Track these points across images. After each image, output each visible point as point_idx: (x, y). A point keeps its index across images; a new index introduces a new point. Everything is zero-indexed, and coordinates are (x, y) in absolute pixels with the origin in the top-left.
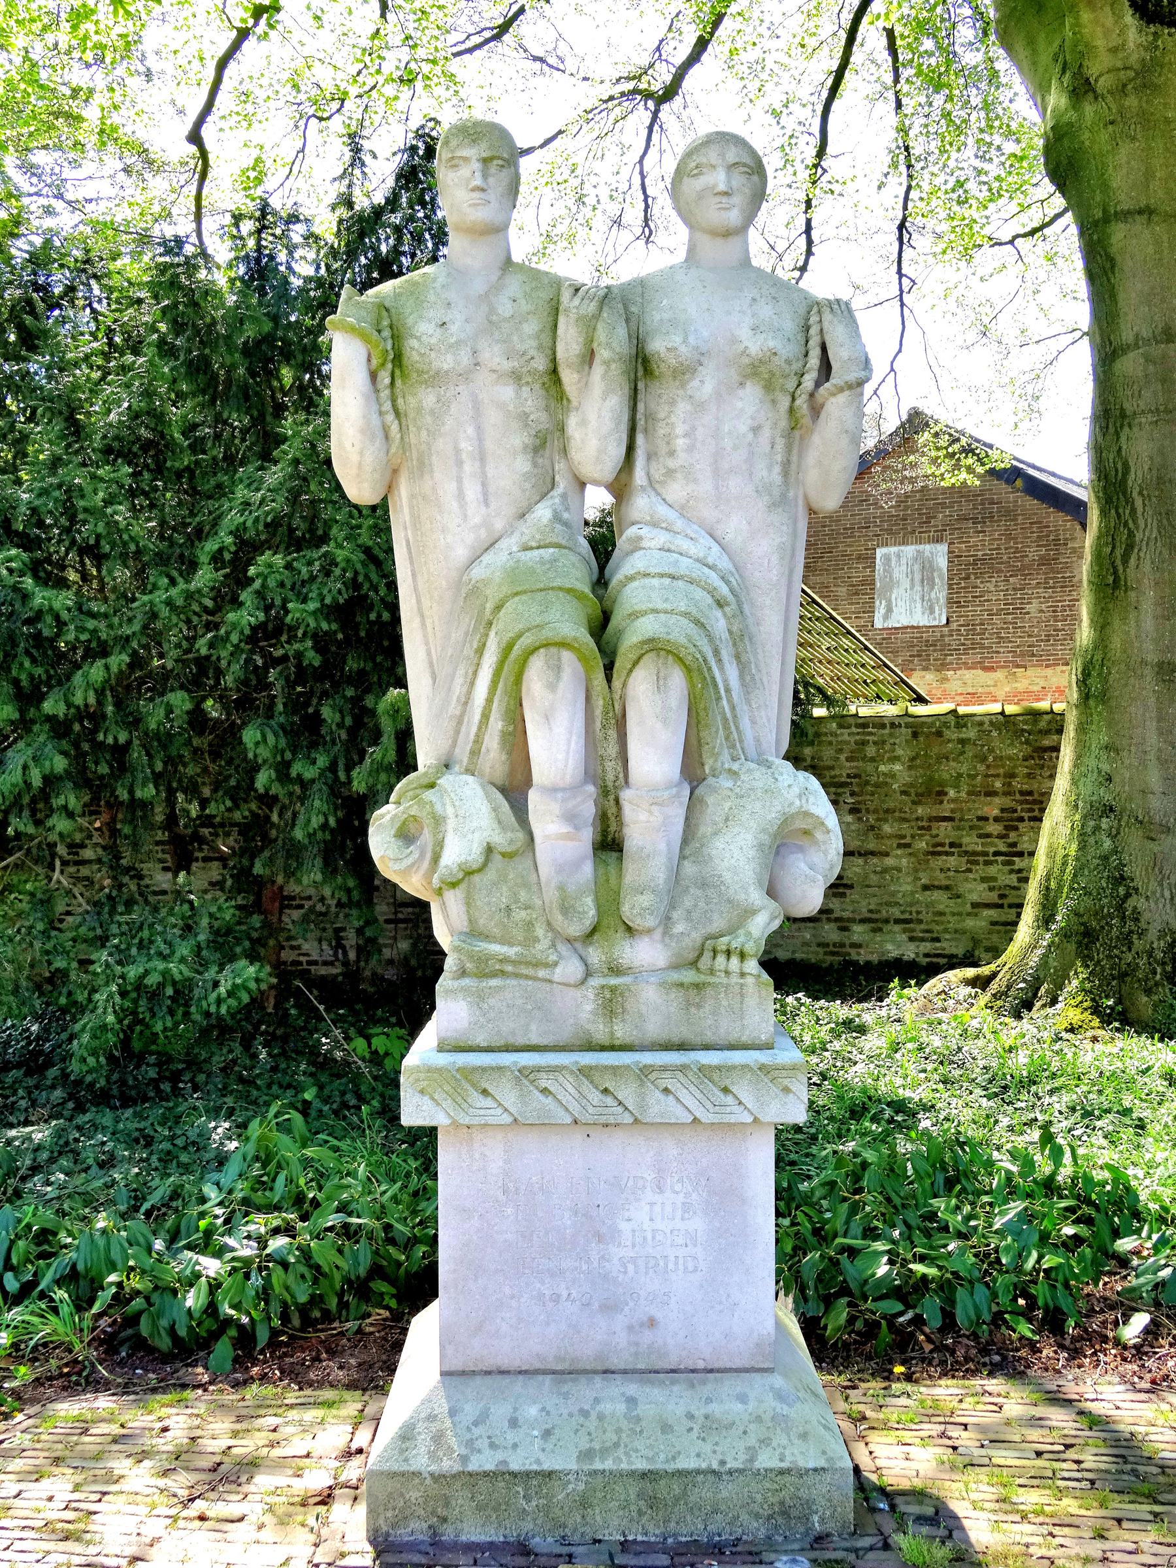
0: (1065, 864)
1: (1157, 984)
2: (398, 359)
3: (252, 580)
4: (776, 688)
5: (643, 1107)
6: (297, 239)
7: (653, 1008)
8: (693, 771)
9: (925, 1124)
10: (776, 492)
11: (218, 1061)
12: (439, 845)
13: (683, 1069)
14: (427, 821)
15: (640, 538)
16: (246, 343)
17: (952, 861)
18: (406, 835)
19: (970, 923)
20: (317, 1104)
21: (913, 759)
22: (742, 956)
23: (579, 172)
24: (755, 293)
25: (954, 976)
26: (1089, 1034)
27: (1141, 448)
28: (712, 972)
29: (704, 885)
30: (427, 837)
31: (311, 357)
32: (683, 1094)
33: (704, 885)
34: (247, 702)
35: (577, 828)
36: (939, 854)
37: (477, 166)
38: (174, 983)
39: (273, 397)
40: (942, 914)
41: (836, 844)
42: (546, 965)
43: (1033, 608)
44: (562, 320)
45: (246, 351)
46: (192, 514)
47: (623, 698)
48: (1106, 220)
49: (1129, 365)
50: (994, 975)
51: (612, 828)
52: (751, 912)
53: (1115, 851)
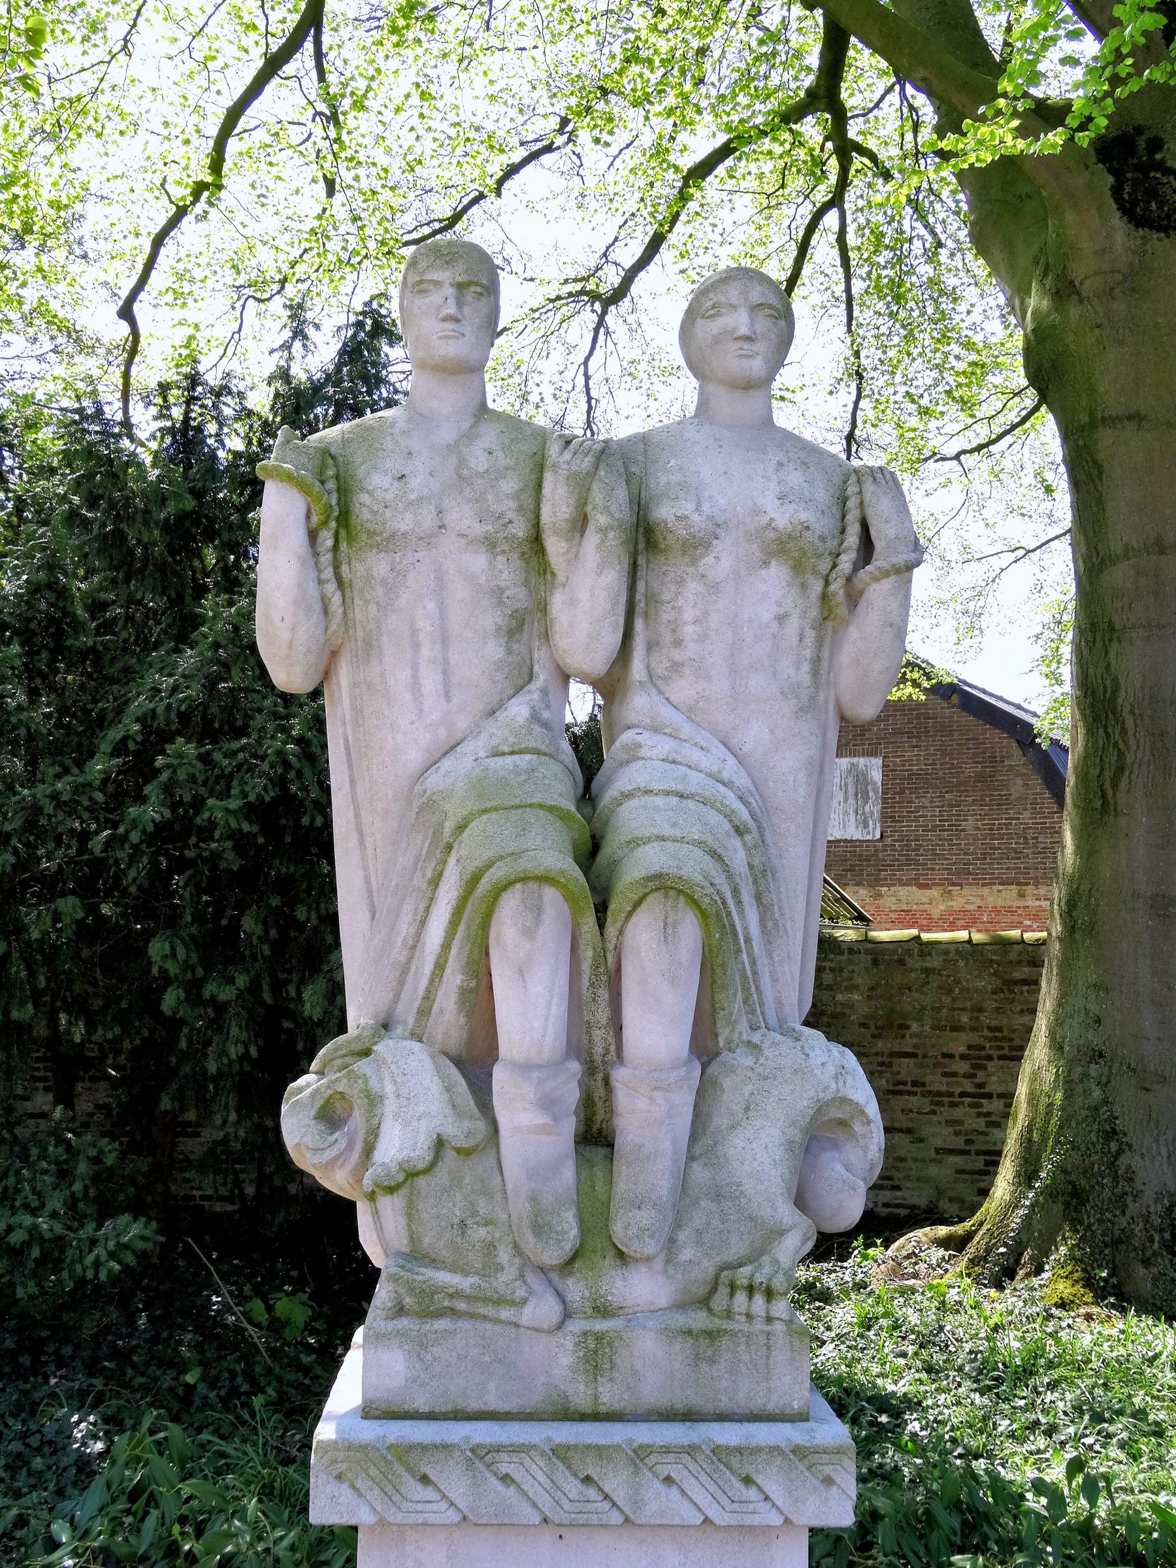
0: (1049, 1114)
1: (1155, 1255)
2: (344, 517)
3: (159, 771)
4: (800, 935)
5: (636, 1503)
6: (228, 411)
7: (651, 1362)
8: (705, 1045)
9: (914, 1426)
10: (805, 695)
11: (88, 1328)
12: (374, 1133)
13: (691, 1450)
14: (359, 1102)
15: (638, 746)
16: (167, 520)
17: (914, 1102)
18: (330, 1116)
19: (933, 1171)
20: (202, 1389)
21: (873, 988)
22: (769, 1294)
23: (523, 369)
24: (781, 456)
25: (922, 1234)
26: (1082, 1311)
27: (1130, 665)
28: (729, 1314)
29: (718, 1196)
30: (357, 1121)
31: (240, 538)
32: (691, 1486)
33: (718, 1196)
34: (152, 906)
35: (556, 1119)
36: (900, 1093)
37: (450, 291)
38: (42, 1240)
39: (194, 579)
40: (902, 1160)
41: (877, 1137)
42: (512, 1303)
43: (969, 824)
44: (548, 478)
45: (166, 527)
46: (95, 701)
47: (618, 949)
48: (1093, 425)
49: (1118, 576)
50: (969, 1237)
51: (600, 1116)
52: (779, 1232)
53: (1106, 1102)
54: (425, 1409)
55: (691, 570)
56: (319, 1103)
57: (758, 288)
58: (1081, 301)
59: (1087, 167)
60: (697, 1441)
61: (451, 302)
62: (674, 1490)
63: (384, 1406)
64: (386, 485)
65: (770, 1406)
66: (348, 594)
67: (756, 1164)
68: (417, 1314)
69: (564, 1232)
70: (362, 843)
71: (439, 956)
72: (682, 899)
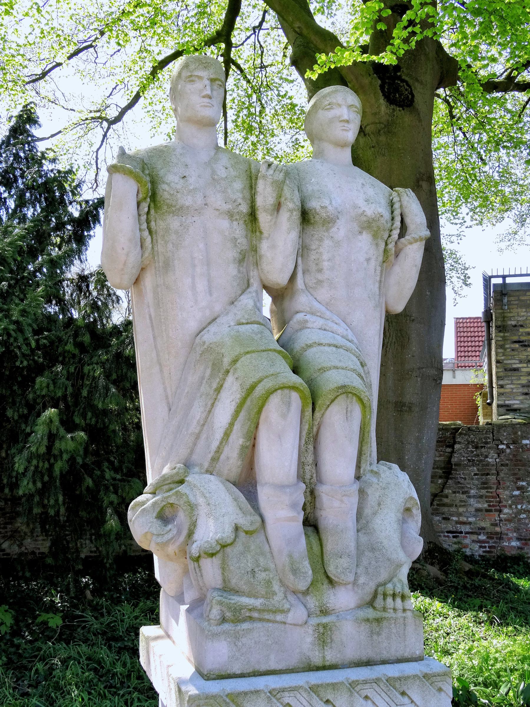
2: (153, 196)
13: (377, 681)
15: (306, 321)
28: (385, 609)
29: (373, 550)
30: (182, 517)
33: (373, 550)
37: (207, 82)
42: (282, 612)
54: (238, 672)
55: (326, 234)
56: (158, 509)
57: (351, 97)
58: (365, 135)
59: (370, 75)
60: (380, 676)
61: (208, 87)
62: (369, 702)
63: (217, 673)
64: (176, 181)
65: (406, 655)
66: (155, 238)
67: (387, 532)
68: (233, 622)
69: (306, 573)
70: (161, 371)
71: (227, 429)
72: (354, 398)
